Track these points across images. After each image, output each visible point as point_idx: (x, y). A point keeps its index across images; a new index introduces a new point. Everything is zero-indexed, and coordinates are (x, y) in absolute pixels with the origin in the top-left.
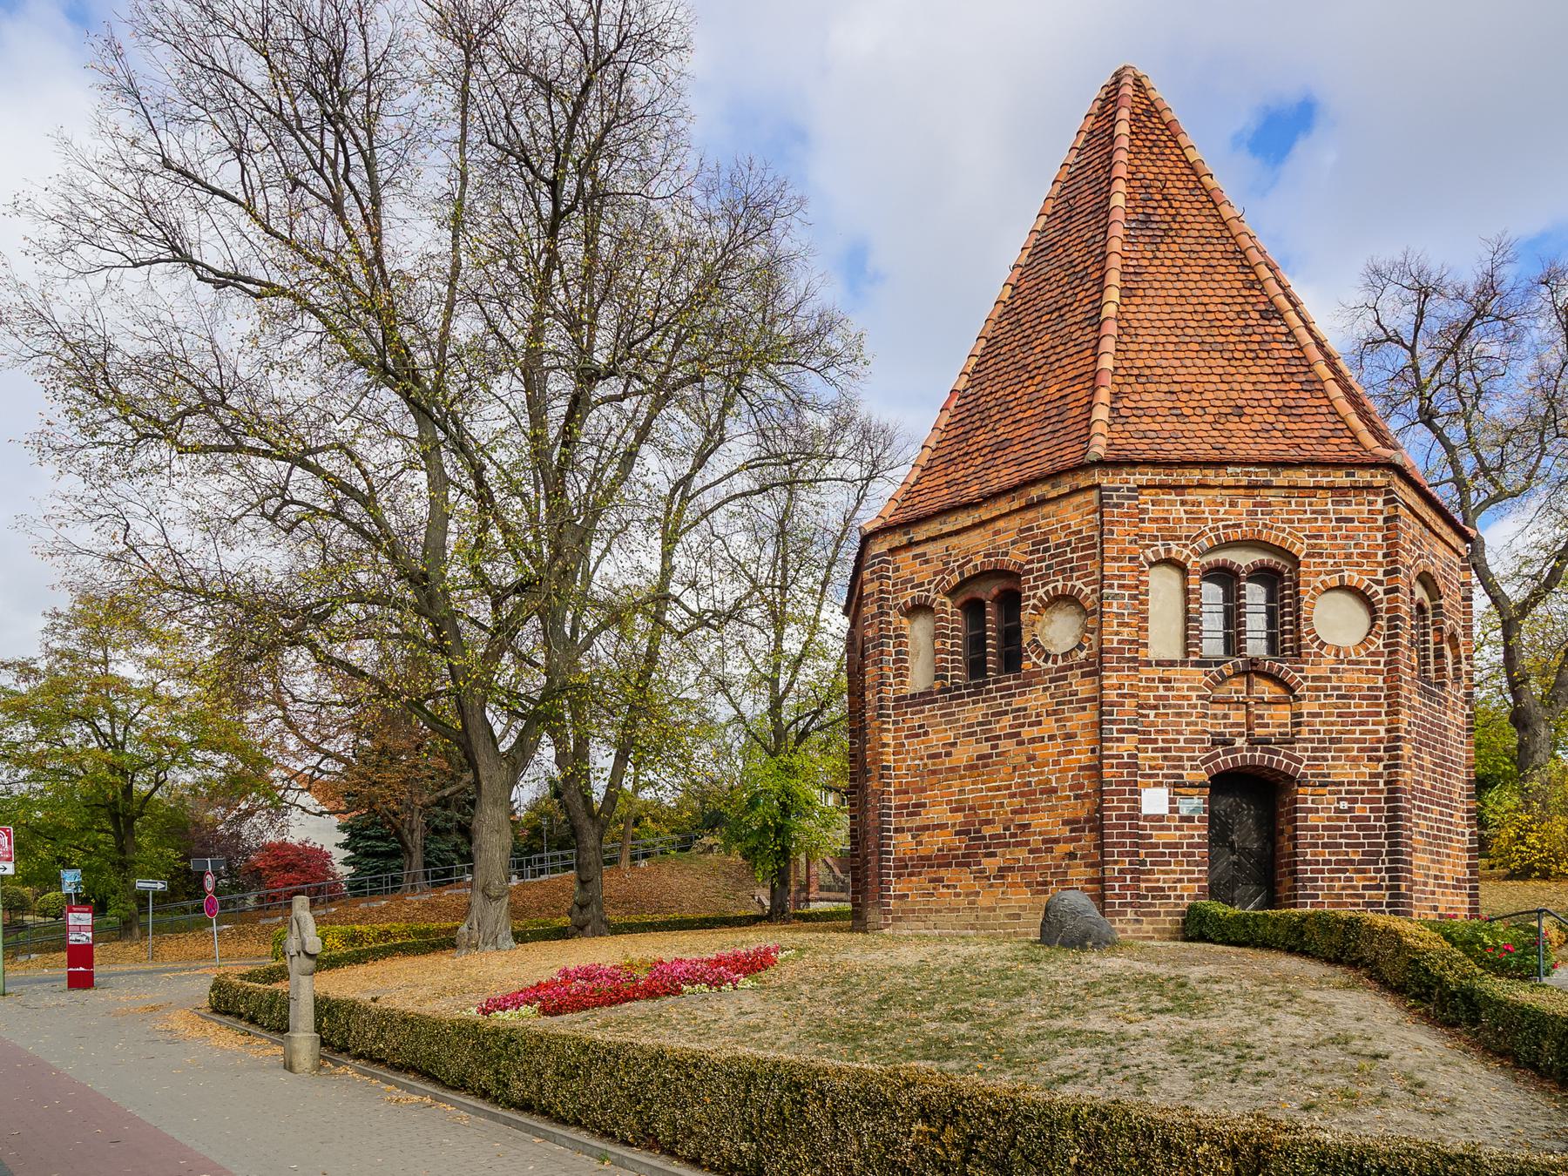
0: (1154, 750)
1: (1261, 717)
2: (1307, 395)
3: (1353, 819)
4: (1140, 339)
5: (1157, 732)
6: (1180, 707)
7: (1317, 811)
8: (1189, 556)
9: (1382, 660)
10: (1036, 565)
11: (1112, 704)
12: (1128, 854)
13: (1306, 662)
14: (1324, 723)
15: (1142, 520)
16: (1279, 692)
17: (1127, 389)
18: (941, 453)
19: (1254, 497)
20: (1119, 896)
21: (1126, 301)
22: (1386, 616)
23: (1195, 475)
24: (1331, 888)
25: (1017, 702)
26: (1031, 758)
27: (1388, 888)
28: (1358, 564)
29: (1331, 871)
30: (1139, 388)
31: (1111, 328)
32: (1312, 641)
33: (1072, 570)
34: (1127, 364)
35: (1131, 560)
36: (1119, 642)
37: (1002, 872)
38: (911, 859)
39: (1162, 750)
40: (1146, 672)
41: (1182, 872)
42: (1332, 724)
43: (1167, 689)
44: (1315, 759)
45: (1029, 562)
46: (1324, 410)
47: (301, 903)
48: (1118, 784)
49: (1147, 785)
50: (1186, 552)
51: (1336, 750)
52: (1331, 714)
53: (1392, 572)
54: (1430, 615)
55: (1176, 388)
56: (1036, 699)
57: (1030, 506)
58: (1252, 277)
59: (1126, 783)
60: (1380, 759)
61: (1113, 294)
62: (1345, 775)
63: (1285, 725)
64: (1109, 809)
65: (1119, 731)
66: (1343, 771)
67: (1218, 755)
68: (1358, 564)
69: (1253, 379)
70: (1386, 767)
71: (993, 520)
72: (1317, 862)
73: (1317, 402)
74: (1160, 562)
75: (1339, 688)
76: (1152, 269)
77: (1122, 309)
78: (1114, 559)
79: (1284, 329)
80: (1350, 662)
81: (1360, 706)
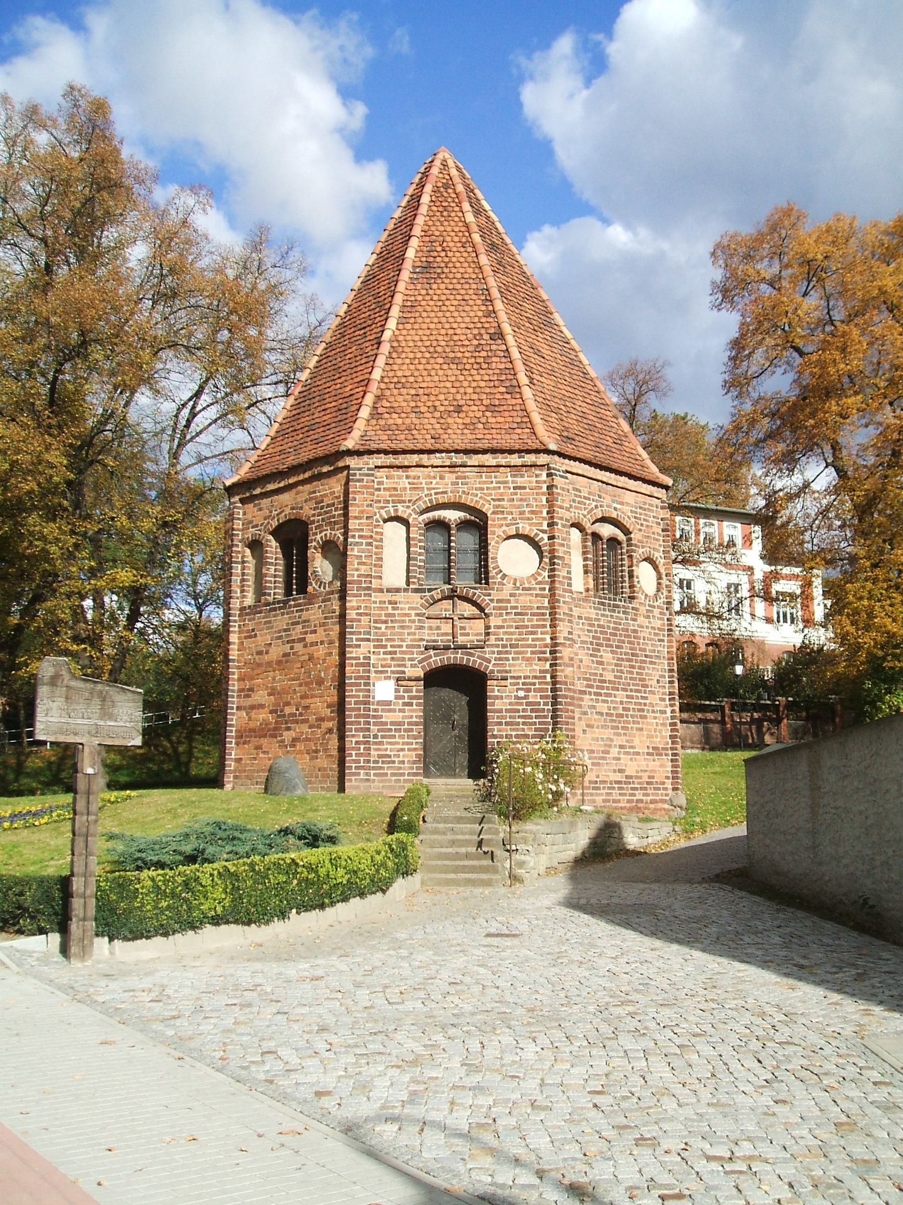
0: (385, 653)
3: (528, 704)
5: (387, 640)
6: (403, 621)
7: (502, 698)
10: (316, 518)
12: (362, 730)
13: (493, 589)
14: (506, 633)
16: (475, 611)
17: (388, 393)
18: (285, 427)
20: (355, 761)
21: (401, 326)
23: (415, 458)
25: (305, 615)
28: (528, 519)
31: (385, 348)
32: (497, 574)
34: (391, 374)
35: (367, 518)
36: (359, 576)
37: (295, 740)
39: (390, 653)
42: (512, 634)
43: (394, 609)
44: (500, 659)
45: (314, 515)
46: (518, 408)
47: (768, 676)
48: (357, 678)
49: (379, 679)
50: (409, 511)
51: (515, 653)
52: (511, 627)
53: (551, 525)
54: (625, 545)
55: (421, 391)
58: (491, 308)
59: (361, 678)
61: (392, 324)
65: (357, 640)
67: (431, 657)
68: (528, 519)
74: (391, 519)
75: (516, 608)
78: (356, 518)
79: (504, 348)
81: (532, 620)
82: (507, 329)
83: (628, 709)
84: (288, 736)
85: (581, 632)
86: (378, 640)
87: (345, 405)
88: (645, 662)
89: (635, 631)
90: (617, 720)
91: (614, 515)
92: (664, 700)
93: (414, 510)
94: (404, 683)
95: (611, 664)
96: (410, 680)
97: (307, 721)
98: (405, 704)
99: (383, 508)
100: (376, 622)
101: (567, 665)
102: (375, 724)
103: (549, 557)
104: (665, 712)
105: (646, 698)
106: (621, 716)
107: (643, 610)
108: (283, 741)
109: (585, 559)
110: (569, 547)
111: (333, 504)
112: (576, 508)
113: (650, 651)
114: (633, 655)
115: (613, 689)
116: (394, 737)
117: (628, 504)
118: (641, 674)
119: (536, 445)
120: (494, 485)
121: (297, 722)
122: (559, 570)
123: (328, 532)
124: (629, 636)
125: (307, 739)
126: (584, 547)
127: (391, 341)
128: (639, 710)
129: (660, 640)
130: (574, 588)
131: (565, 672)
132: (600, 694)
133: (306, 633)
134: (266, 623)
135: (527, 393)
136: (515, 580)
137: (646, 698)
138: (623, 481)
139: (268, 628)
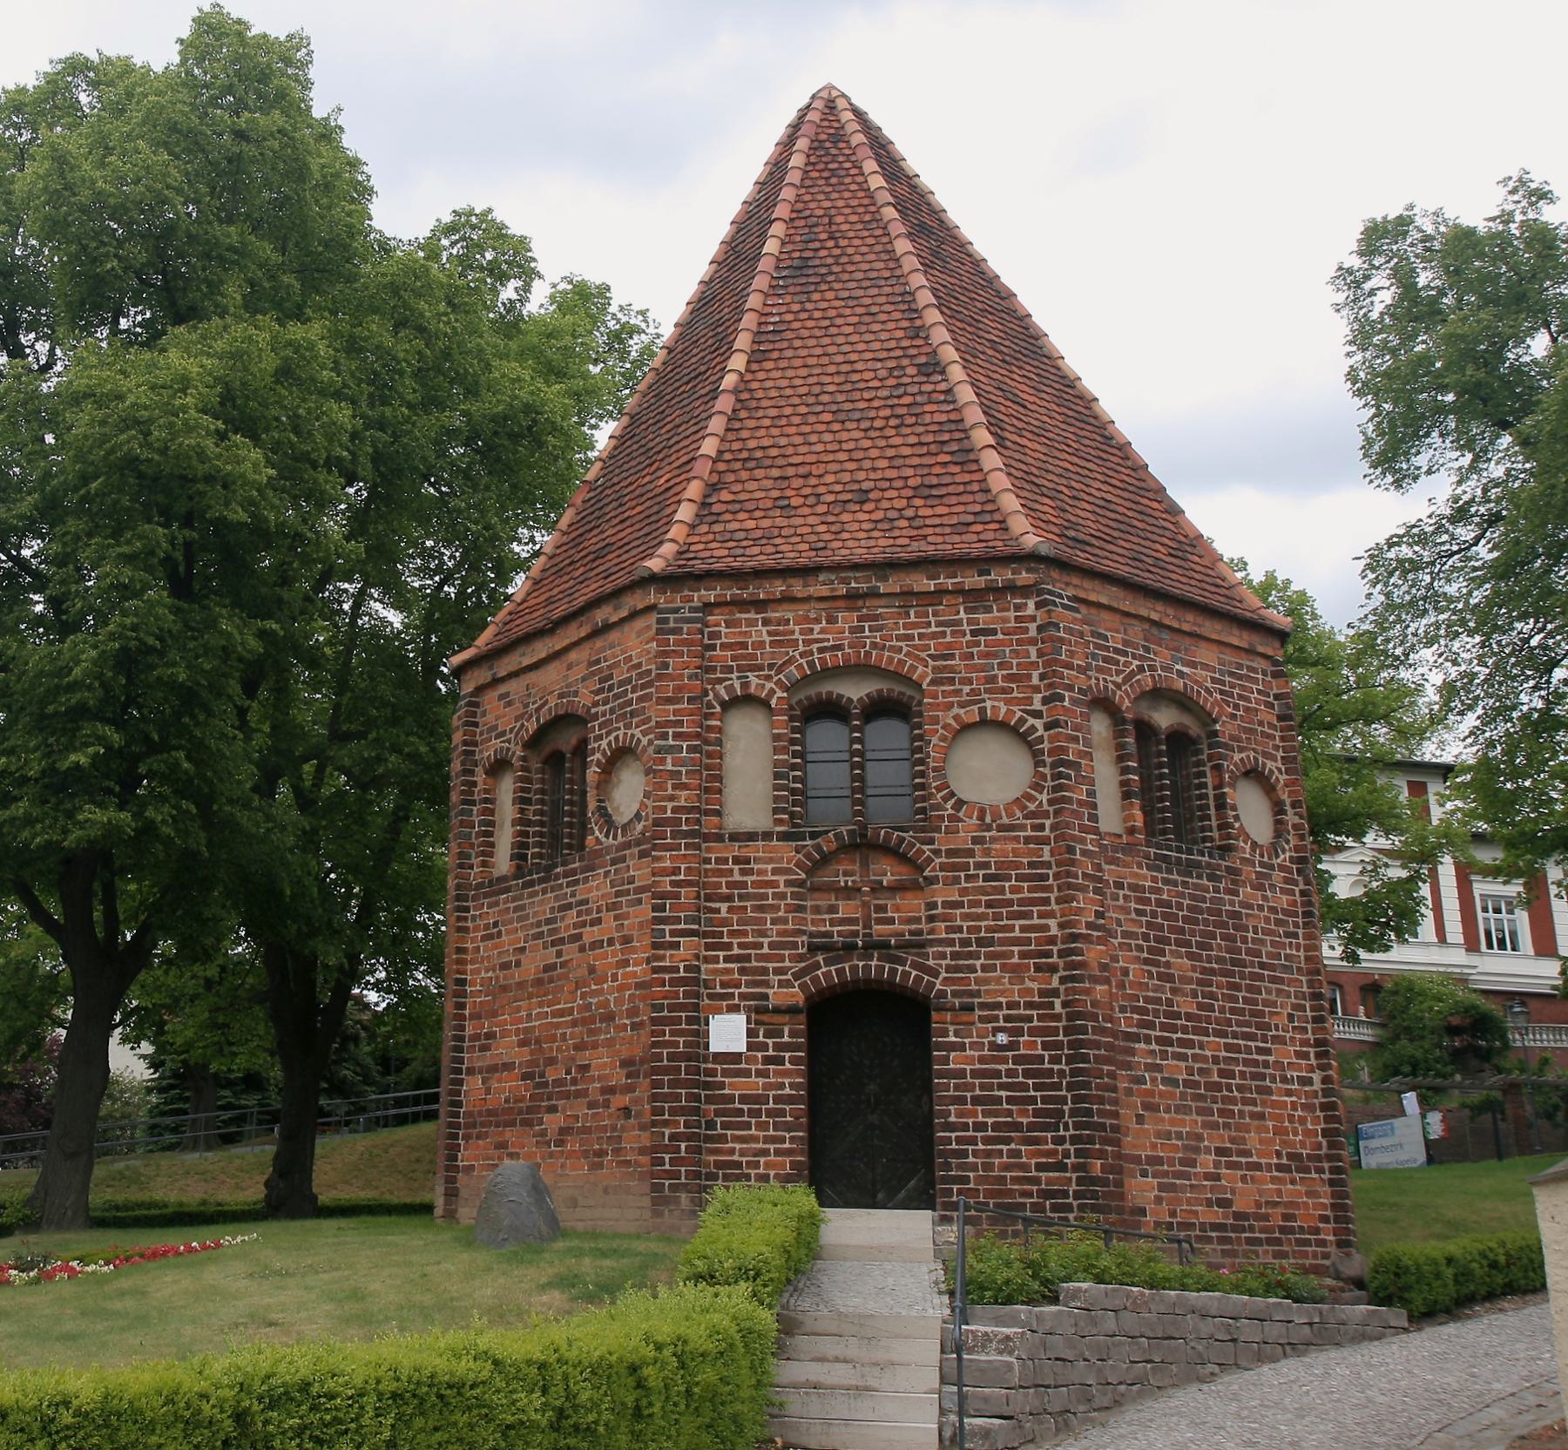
0: (727, 959)
1: (881, 909)
2: (957, 469)
3: (1018, 1060)
4: (760, 413)
5: (732, 933)
6: (764, 897)
7: (962, 1047)
8: (772, 692)
9: (1048, 823)
14: (966, 917)
15: (713, 647)
17: (730, 477)
19: (859, 609)
21: (755, 367)
22: (1049, 760)
23: (778, 588)
24: (988, 1167)
26: (592, 970)
27: (1076, 1168)
28: (1004, 691)
29: (986, 1140)
30: (744, 475)
31: (725, 403)
32: (945, 799)
33: (632, 714)
38: (480, 1113)
39: (737, 958)
40: (715, 852)
41: (767, 1140)
43: (743, 872)
44: (957, 969)
48: (672, 1008)
49: (719, 1011)
50: (769, 685)
51: (988, 956)
52: (976, 904)
55: (791, 471)
56: (597, 888)
57: (596, 633)
59: (682, 1008)
60: (1053, 969)
61: (738, 362)
62: (1002, 993)
63: (918, 920)
65: (673, 933)
66: (1002, 988)
67: (817, 966)
68: (1004, 691)
69: (890, 452)
70: (1063, 980)
72: (965, 1127)
75: (986, 865)
76: (796, 325)
77: (748, 377)
80: (1001, 828)
83: (1231, 1075)
84: (552, 1122)
85: (1124, 917)
87: (655, 509)
88: (1261, 978)
89: (1235, 915)
90: (1207, 1094)
92: (1305, 1056)
94: (765, 1018)
95: (1190, 981)
96: (777, 1010)
98: (768, 1060)
99: (720, 681)
101: (1095, 980)
105: (1268, 1052)
106: (1217, 1087)
108: (543, 1133)
109: (1125, 771)
110: (1087, 743)
111: (629, 680)
112: (1100, 670)
113: (1270, 955)
114: (1234, 962)
115: (1196, 1031)
116: (748, 1126)
117: (1205, 667)
120: (934, 629)
121: (566, 1096)
123: (621, 733)
124: (1224, 925)
125: (586, 1130)
126: (1120, 747)
127: (736, 391)
128: (1254, 1076)
129: (1288, 935)
130: (1104, 826)
132: (1170, 1042)
133: (584, 924)
134: (516, 909)
135: (991, 460)
136: (982, 812)
137: (1268, 1052)
138: (1189, 622)
139: (520, 919)
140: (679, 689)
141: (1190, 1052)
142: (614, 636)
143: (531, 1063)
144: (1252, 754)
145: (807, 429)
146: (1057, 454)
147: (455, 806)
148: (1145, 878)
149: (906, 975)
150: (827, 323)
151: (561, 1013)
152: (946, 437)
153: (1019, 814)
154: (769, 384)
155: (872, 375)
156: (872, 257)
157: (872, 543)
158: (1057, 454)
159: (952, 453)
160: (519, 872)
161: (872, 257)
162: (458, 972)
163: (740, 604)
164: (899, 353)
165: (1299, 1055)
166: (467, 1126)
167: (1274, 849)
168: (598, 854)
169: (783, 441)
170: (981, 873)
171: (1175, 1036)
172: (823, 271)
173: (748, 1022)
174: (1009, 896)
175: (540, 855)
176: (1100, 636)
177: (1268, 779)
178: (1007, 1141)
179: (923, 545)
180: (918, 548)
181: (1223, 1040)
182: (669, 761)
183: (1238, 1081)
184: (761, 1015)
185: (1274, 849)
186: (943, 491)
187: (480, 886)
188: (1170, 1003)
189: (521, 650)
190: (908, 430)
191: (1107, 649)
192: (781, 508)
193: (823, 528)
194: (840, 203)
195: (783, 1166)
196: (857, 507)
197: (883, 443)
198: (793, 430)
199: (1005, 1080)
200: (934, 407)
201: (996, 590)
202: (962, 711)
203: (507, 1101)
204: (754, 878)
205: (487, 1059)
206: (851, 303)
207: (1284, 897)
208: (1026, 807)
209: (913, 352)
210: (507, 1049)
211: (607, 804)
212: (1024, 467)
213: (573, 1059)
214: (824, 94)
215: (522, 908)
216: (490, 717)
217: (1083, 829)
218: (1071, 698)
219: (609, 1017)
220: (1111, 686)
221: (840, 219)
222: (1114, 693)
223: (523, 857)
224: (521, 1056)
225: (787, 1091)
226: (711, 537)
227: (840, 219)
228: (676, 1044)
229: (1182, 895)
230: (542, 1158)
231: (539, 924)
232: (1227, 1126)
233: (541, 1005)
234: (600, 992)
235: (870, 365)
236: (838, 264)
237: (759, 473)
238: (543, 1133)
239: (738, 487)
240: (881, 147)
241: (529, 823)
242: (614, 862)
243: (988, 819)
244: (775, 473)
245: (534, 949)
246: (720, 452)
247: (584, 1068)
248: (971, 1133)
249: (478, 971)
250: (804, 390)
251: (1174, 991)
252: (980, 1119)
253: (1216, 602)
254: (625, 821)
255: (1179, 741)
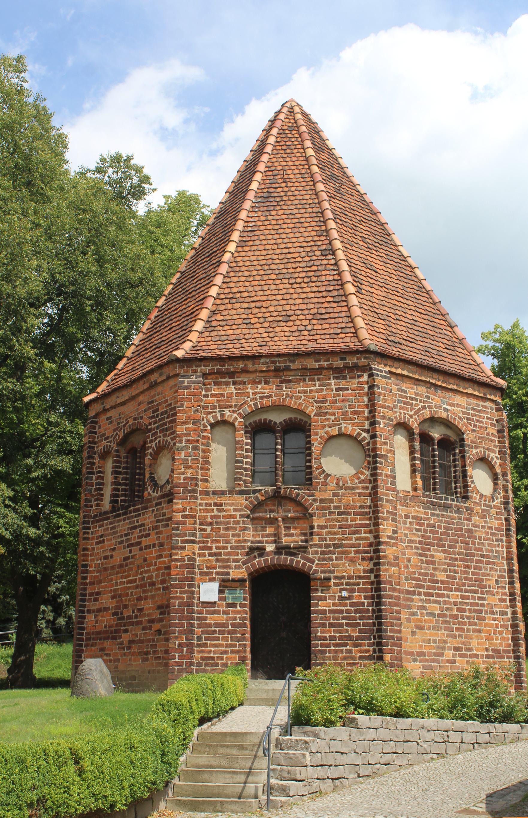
0: (210, 555)
2: (335, 305)
3: (351, 605)
5: (213, 542)
6: (229, 523)
10: (153, 426)
11: (178, 523)
13: (316, 489)
14: (329, 533)
17: (223, 307)
19: (281, 377)
21: (240, 249)
23: (241, 365)
25: (142, 520)
28: (351, 419)
29: (336, 645)
31: (224, 269)
32: (320, 474)
33: (167, 429)
39: (215, 554)
42: (335, 533)
50: (235, 415)
51: (339, 553)
52: (333, 526)
55: (253, 305)
59: (186, 579)
61: (232, 247)
64: (173, 598)
65: (182, 542)
68: (351, 419)
69: (303, 296)
71: (138, 395)
72: (325, 638)
73: (340, 309)
75: (339, 507)
76: (262, 228)
77: (236, 255)
78: (183, 423)
82: (338, 244)
83: (464, 611)
86: (203, 542)
87: (186, 323)
88: (482, 562)
89: (470, 531)
90: (452, 621)
91: (444, 415)
93: (240, 414)
95: (444, 564)
96: (233, 580)
97: (138, 623)
98: (229, 605)
100: (201, 524)
102: (199, 626)
103: (372, 457)
104: (506, 613)
106: (456, 617)
107: (477, 509)
111: (166, 412)
112: (402, 408)
114: (467, 555)
116: (218, 639)
117: (459, 406)
118: (478, 574)
119: (356, 346)
121: (132, 624)
122: (381, 469)
123: (161, 439)
124: (463, 536)
125: (141, 641)
128: (476, 611)
129: (497, 540)
130: (399, 487)
131: (388, 572)
133: (141, 537)
135: (354, 300)
139: (114, 533)
140: (189, 417)
141: (442, 600)
142: (159, 389)
143: (118, 607)
144: (482, 450)
145: (263, 283)
146: (391, 296)
147: (84, 475)
148: (421, 513)
149: (298, 562)
150: (278, 227)
151: (131, 582)
152: (332, 288)
153: (356, 481)
154: (246, 259)
155: (298, 255)
156: (304, 193)
157: (289, 343)
158: (391, 296)
159: (333, 297)
160: (114, 509)
161: (304, 193)
162: (84, 561)
163: (220, 373)
164: (312, 243)
165: (501, 600)
166: (87, 639)
167: (492, 498)
168: (149, 501)
169: (250, 289)
170: (337, 511)
171: (434, 592)
172: (278, 199)
173: (220, 586)
174: (349, 523)
175: (124, 501)
176: (402, 391)
177: (490, 462)
178: (345, 645)
179: (314, 344)
180: (312, 346)
181: (460, 593)
182: (183, 454)
183: (467, 614)
184: (226, 585)
185: (492, 498)
186: (327, 316)
187: (95, 516)
188: (432, 575)
189: (117, 394)
190: (313, 284)
191: (406, 397)
192: (247, 324)
193: (265, 335)
194: (290, 163)
195: (235, 658)
196: (284, 324)
197: (300, 290)
198: (256, 283)
199: (345, 614)
200: (327, 272)
201: (349, 368)
202: (330, 429)
203: (105, 627)
204: (224, 513)
205: (95, 606)
206: (291, 217)
207: (497, 522)
208: (359, 478)
209: (319, 243)
210: (106, 600)
211: (155, 475)
212: (371, 304)
213: (136, 605)
214: (288, 105)
215: (114, 528)
216: (102, 429)
217: (388, 489)
218: (384, 423)
219: (153, 584)
220: (407, 416)
221: (289, 172)
222: (409, 420)
223: (117, 502)
224: (112, 604)
225: (238, 621)
226: (210, 339)
227: (289, 172)
228: (182, 598)
229: (441, 521)
230: (121, 656)
231: (122, 536)
232: (460, 636)
233: (122, 577)
234: (149, 571)
235: (298, 249)
236: (286, 196)
237: (237, 306)
238: (121, 643)
239: (226, 312)
240: (315, 132)
241: (119, 484)
242: (157, 505)
243: (341, 484)
244: (245, 305)
245: (119, 549)
246: (219, 294)
247: (141, 610)
248: (328, 642)
249: (93, 560)
250: (264, 262)
251: (435, 569)
252: (333, 634)
253: (468, 373)
254: (163, 483)
255: (445, 444)
